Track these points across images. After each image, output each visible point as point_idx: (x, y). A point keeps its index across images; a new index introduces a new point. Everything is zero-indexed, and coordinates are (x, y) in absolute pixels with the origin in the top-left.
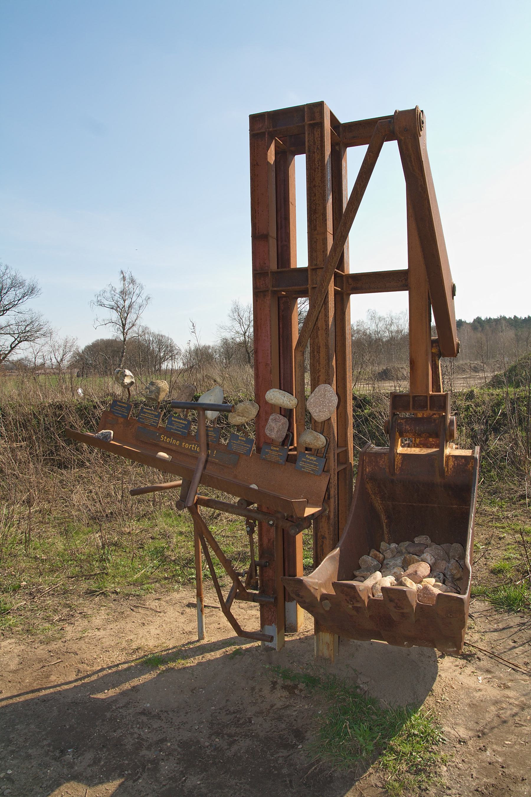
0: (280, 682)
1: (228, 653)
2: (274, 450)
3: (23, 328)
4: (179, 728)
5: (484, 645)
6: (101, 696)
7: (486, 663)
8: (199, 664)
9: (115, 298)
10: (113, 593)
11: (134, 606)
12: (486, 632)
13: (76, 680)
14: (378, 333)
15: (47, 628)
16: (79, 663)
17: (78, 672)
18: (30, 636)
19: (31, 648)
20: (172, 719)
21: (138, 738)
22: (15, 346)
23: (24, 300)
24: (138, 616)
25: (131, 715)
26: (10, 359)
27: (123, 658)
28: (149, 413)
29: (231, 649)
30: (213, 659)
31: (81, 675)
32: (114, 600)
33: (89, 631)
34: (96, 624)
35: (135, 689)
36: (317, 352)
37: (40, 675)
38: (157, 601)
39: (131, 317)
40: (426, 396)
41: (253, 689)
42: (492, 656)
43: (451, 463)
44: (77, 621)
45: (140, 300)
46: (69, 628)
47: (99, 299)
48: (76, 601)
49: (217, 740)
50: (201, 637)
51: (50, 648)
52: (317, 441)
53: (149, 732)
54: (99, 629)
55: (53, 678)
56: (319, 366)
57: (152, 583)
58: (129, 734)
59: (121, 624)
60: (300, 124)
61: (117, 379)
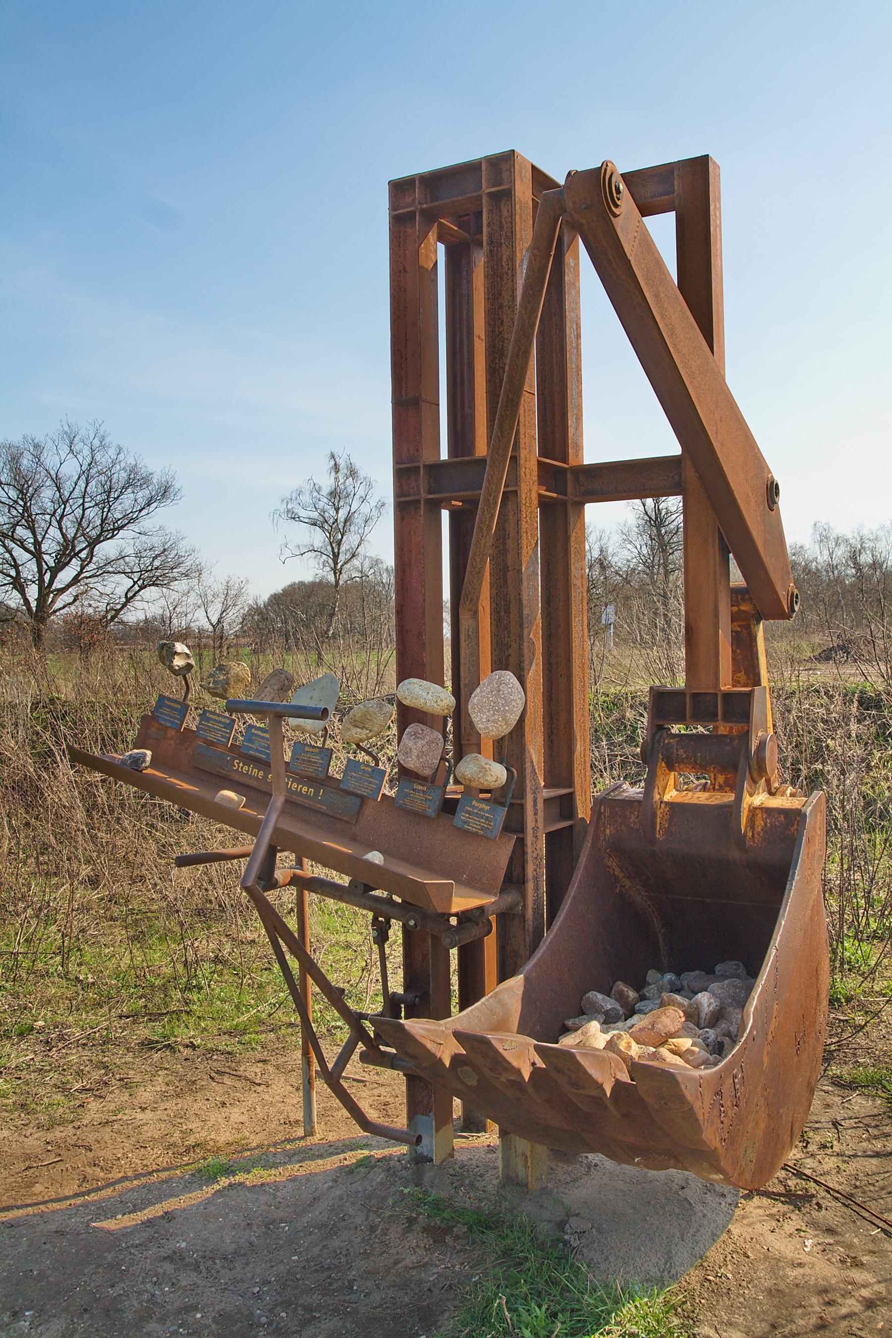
3: (148, 562)
4: (225, 1289)
5: (842, 1180)
6: (109, 1224)
7: (833, 1213)
9: (321, 505)
10: (187, 1046)
12: (855, 1156)
13: (76, 1195)
14: (833, 568)
15: (56, 1102)
16: (89, 1165)
17: (83, 1181)
18: (23, 1115)
19: (20, 1135)
20: (218, 1272)
21: (148, 1301)
22: (134, 595)
23: (151, 509)
25: (148, 1261)
26: (125, 619)
27: (164, 1161)
28: (215, 721)
29: (352, 1158)
31: (87, 1186)
33: (126, 1112)
34: (143, 1100)
35: (168, 1216)
36: (505, 612)
37: (18, 1182)
39: (350, 541)
40: (716, 694)
41: (373, 1229)
42: (847, 1199)
43: (759, 823)
45: (365, 509)
46: (94, 1105)
47: (290, 506)
48: (118, 1057)
49: (284, 1314)
50: (310, 1133)
51: (50, 1137)
52: (485, 775)
53: (171, 1292)
54: (143, 1109)
55: (38, 1188)
56: (509, 637)
57: (262, 1032)
58: (136, 1292)
59: (186, 1102)
60: (475, 194)
61: (162, 659)
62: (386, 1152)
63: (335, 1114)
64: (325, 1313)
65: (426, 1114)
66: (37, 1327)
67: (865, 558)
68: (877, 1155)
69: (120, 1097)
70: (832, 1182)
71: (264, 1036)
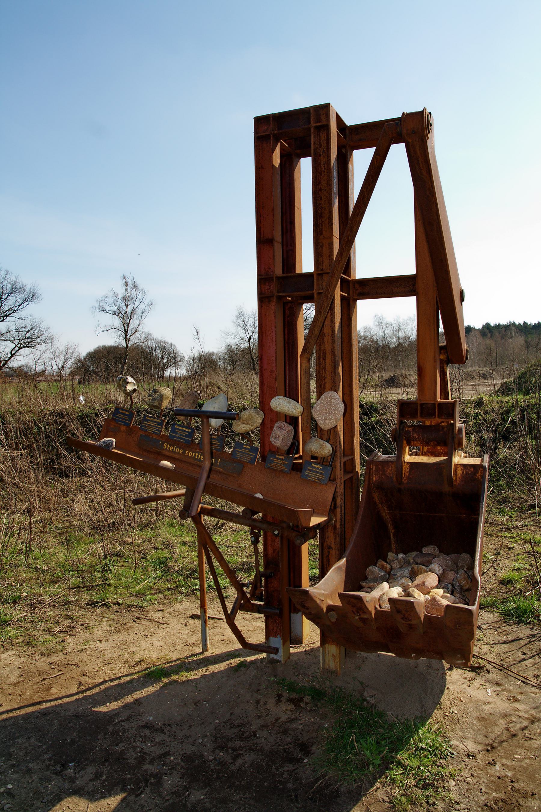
0: (286, 694)
1: (232, 665)
2: (279, 459)
3: (23, 334)
4: (182, 742)
5: (494, 657)
6: (103, 709)
7: (495, 675)
8: (203, 676)
10: (115, 604)
11: (137, 618)
12: (495, 644)
13: (78, 693)
14: (385, 339)
16: (81, 675)
18: (30, 648)
19: (32, 660)
21: (140, 752)
22: (16, 353)
23: (25, 305)
24: (140, 628)
26: (11, 366)
27: (125, 671)
28: (152, 421)
29: (235, 662)
30: (217, 671)
31: (82, 688)
32: (116, 612)
33: (91, 643)
34: (98, 636)
35: (137, 702)
36: (323, 359)
37: (40, 688)
38: (160, 612)
39: (134, 323)
41: (258, 702)
42: (502, 668)
43: (459, 472)
44: (79, 632)
45: (142, 306)
46: (70, 640)
47: (101, 304)
48: (77, 612)
49: (221, 754)
50: (205, 649)
51: (51, 660)
53: (152, 746)
54: (100, 641)
55: (54, 691)
56: (325, 373)
57: (154, 594)
58: (132, 747)
59: (124, 636)
60: (306, 126)
61: (119, 386)
62: (253, 658)
63: (214, 638)
64: (245, 751)
65: (275, 636)
66: (79, 772)
67: (401, 334)
68: (505, 642)
69: (82, 635)
70: (490, 657)
71: (156, 596)
